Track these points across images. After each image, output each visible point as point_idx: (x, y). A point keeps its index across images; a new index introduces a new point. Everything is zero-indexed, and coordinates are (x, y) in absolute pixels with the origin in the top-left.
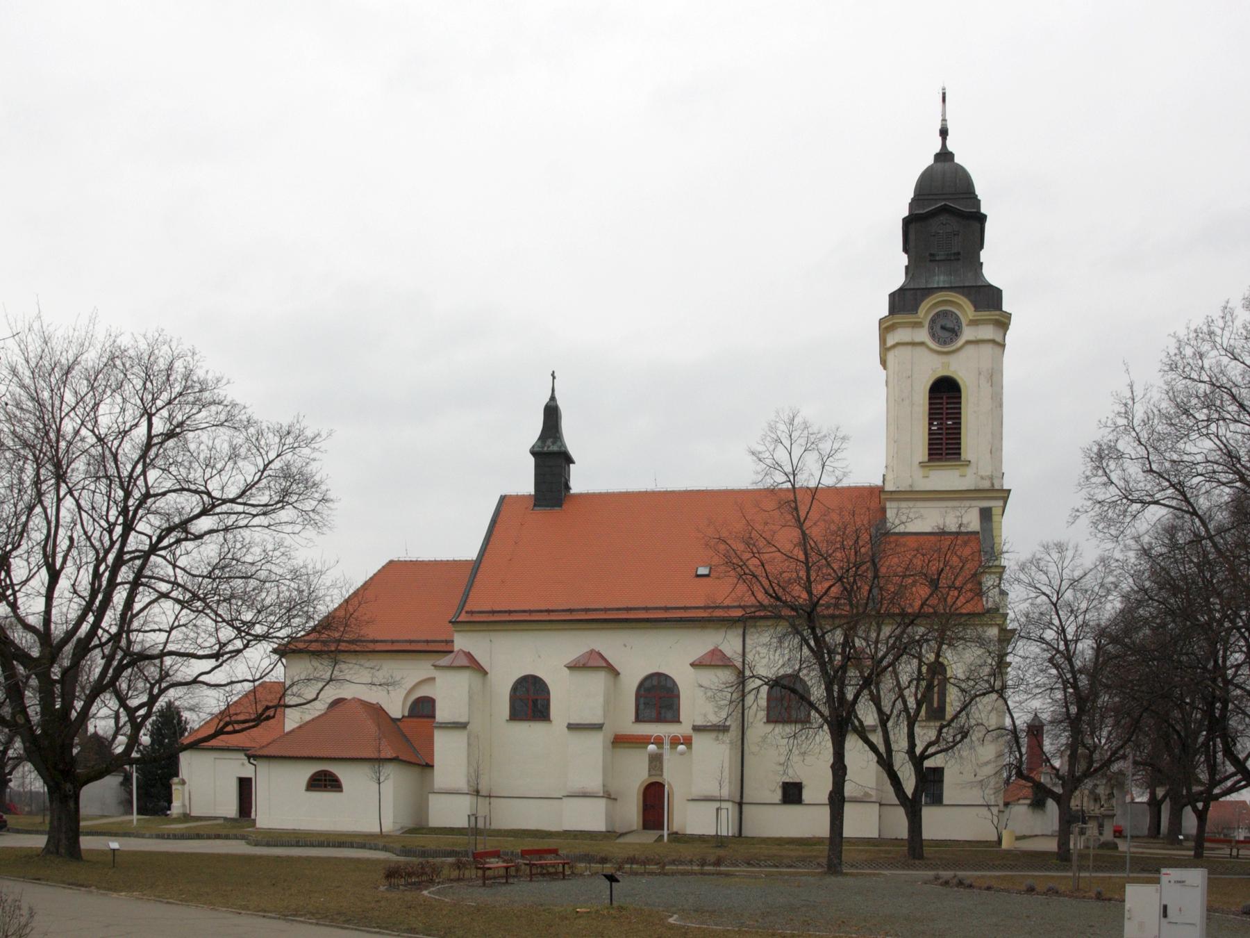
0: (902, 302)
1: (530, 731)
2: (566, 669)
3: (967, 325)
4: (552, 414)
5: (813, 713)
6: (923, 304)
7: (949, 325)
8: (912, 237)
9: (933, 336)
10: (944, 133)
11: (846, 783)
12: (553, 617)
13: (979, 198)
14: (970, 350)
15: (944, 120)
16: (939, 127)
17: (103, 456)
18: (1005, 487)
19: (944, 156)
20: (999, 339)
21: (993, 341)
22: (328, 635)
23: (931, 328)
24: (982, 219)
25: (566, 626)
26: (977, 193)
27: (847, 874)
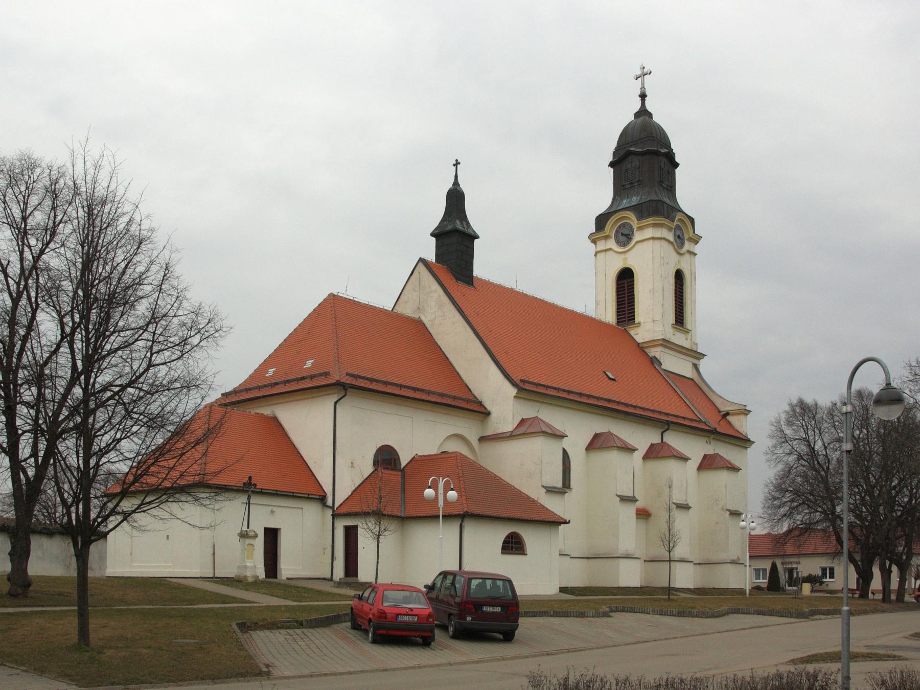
0: (601, 221)
4: (455, 198)
9: (618, 242)
10: (643, 96)
12: (571, 397)
13: (674, 151)
14: (638, 246)
15: (456, 177)
19: (643, 113)
22: (882, 607)
23: (616, 237)
25: (586, 409)
26: (672, 148)
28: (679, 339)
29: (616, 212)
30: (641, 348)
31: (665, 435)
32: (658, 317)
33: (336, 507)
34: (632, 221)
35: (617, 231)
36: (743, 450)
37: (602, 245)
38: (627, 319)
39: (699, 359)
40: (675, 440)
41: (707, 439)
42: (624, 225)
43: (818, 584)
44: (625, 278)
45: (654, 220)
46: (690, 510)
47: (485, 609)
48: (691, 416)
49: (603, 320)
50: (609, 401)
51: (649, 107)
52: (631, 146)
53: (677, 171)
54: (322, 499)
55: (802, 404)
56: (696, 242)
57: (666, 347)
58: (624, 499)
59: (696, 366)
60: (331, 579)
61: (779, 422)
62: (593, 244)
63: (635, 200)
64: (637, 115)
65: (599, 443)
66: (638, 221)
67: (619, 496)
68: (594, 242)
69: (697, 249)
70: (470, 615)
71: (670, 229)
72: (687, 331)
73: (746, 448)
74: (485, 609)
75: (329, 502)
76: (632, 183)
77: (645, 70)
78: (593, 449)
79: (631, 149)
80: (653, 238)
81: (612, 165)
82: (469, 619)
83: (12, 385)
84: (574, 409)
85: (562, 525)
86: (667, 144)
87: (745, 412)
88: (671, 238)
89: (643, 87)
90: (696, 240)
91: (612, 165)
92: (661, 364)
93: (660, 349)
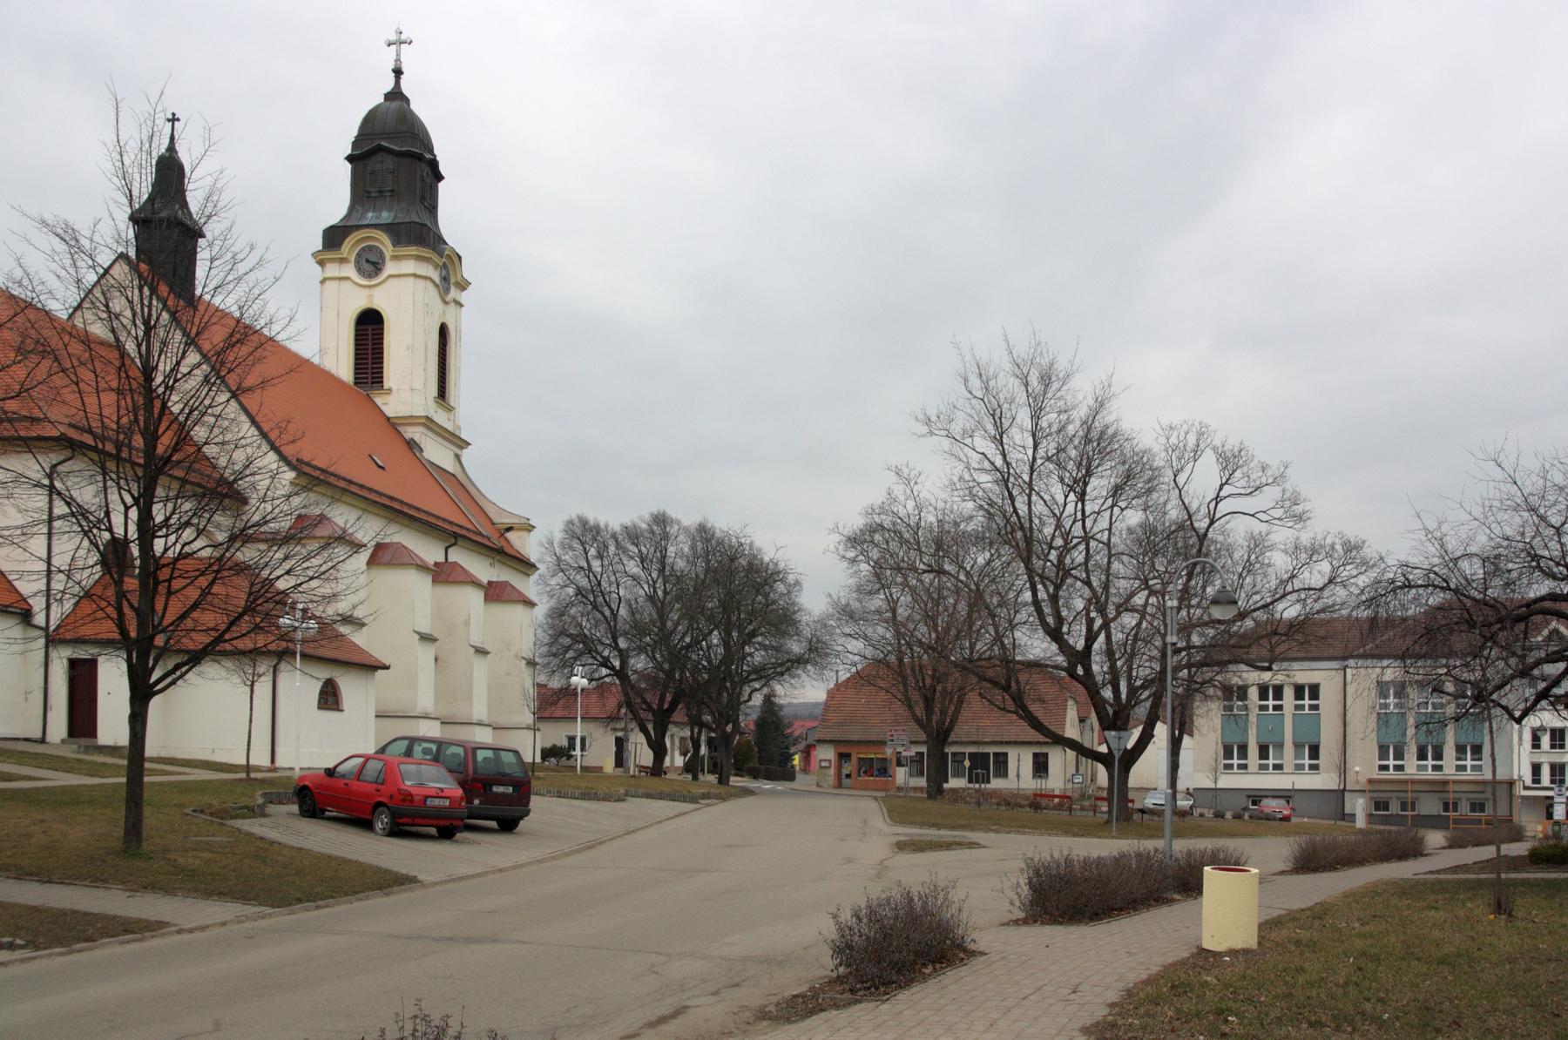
0: (334, 237)
1: (1249, 767)
2: (386, 661)
5: (136, 605)
6: (348, 240)
9: (359, 270)
10: (398, 72)
14: (392, 282)
15: (172, 138)
16: (392, 66)
17: (292, 641)
19: (396, 95)
23: (357, 263)
28: (441, 418)
29: (359, 227)
30: (393, 424)
31: (450, 550)
32: (418, 385)
33: (52, 629)
34: (383, 244)
35: (359, 255)
36: (526, 578)
37: (333, 270)
38: (370, 380)
39: (462, 448)
40: (460, 556)
41: (491, 560)
43: (564, 758)
44: (370, 325)
45: (418, 251)
46: (489, 656)
47: (495, 789)
48: (469, 526)
49: (334, 371)
50: (392, 499)
51: (406, 88)
52: (382, 139)
53: (441, 185)
54: (26, 616)
55: (584, 522)
56: (463, 289)
57: (428, 428)
58: (426, 638)
59: (458, 457)
60: (43, 741)
61: (551, 543)
62: (319, 268)
63: (386, 217)
64: (389, 96)
65: (386, 557)
66: (394, 246)
67: (418, 633)
68: (321, 263)
69: (464, 297)
70: (477, 797)
71: (436, 266)
72: (450, 409)
73: (528, 575)
74: (495, 789)
75: (40, 619)
76: (383, 192)
77: (403, 37)
78: (379, 564)
79: (383, 143)
80: (415, 276)
81: (350, 159)
82: (476, 802)
85: (379, 671)
86: (429, 148)
87: (530, 528)
88: (437, 279)
89: (398, 60)
90: (463, 285)
91: (350, 159)
92: (421, 450)
93: (421, 429)
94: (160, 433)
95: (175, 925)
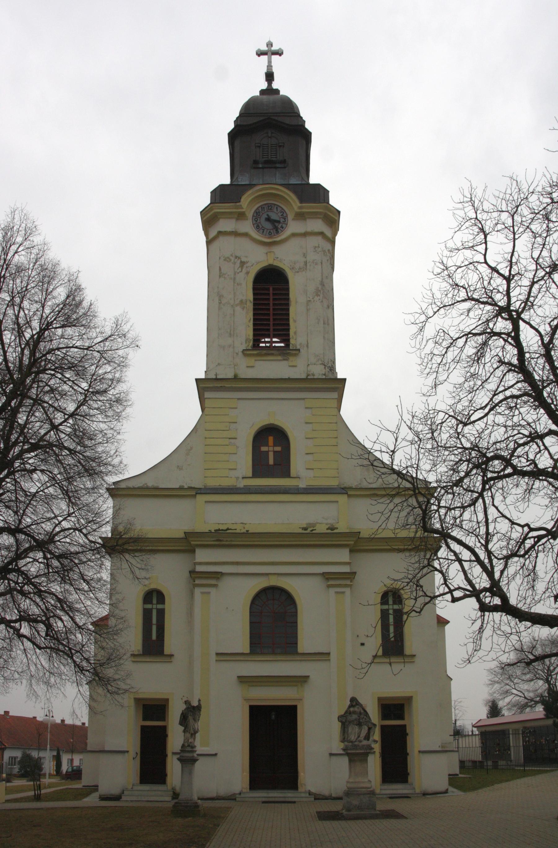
3: (293, 219)
7: (274, 216)
8: (237, 150)
9: (258, 227)
11: (481, 570)
16: (265, 70)
18: (339, 376)
20: (329, 234)
21: (322, 234)
24: (306, 136)
27: (192, 594)
42: (270, 207)
83: (12, 386)
84: (157, 662)
89: (270, 66)
94: (47, 372)
95: (65, 690)
